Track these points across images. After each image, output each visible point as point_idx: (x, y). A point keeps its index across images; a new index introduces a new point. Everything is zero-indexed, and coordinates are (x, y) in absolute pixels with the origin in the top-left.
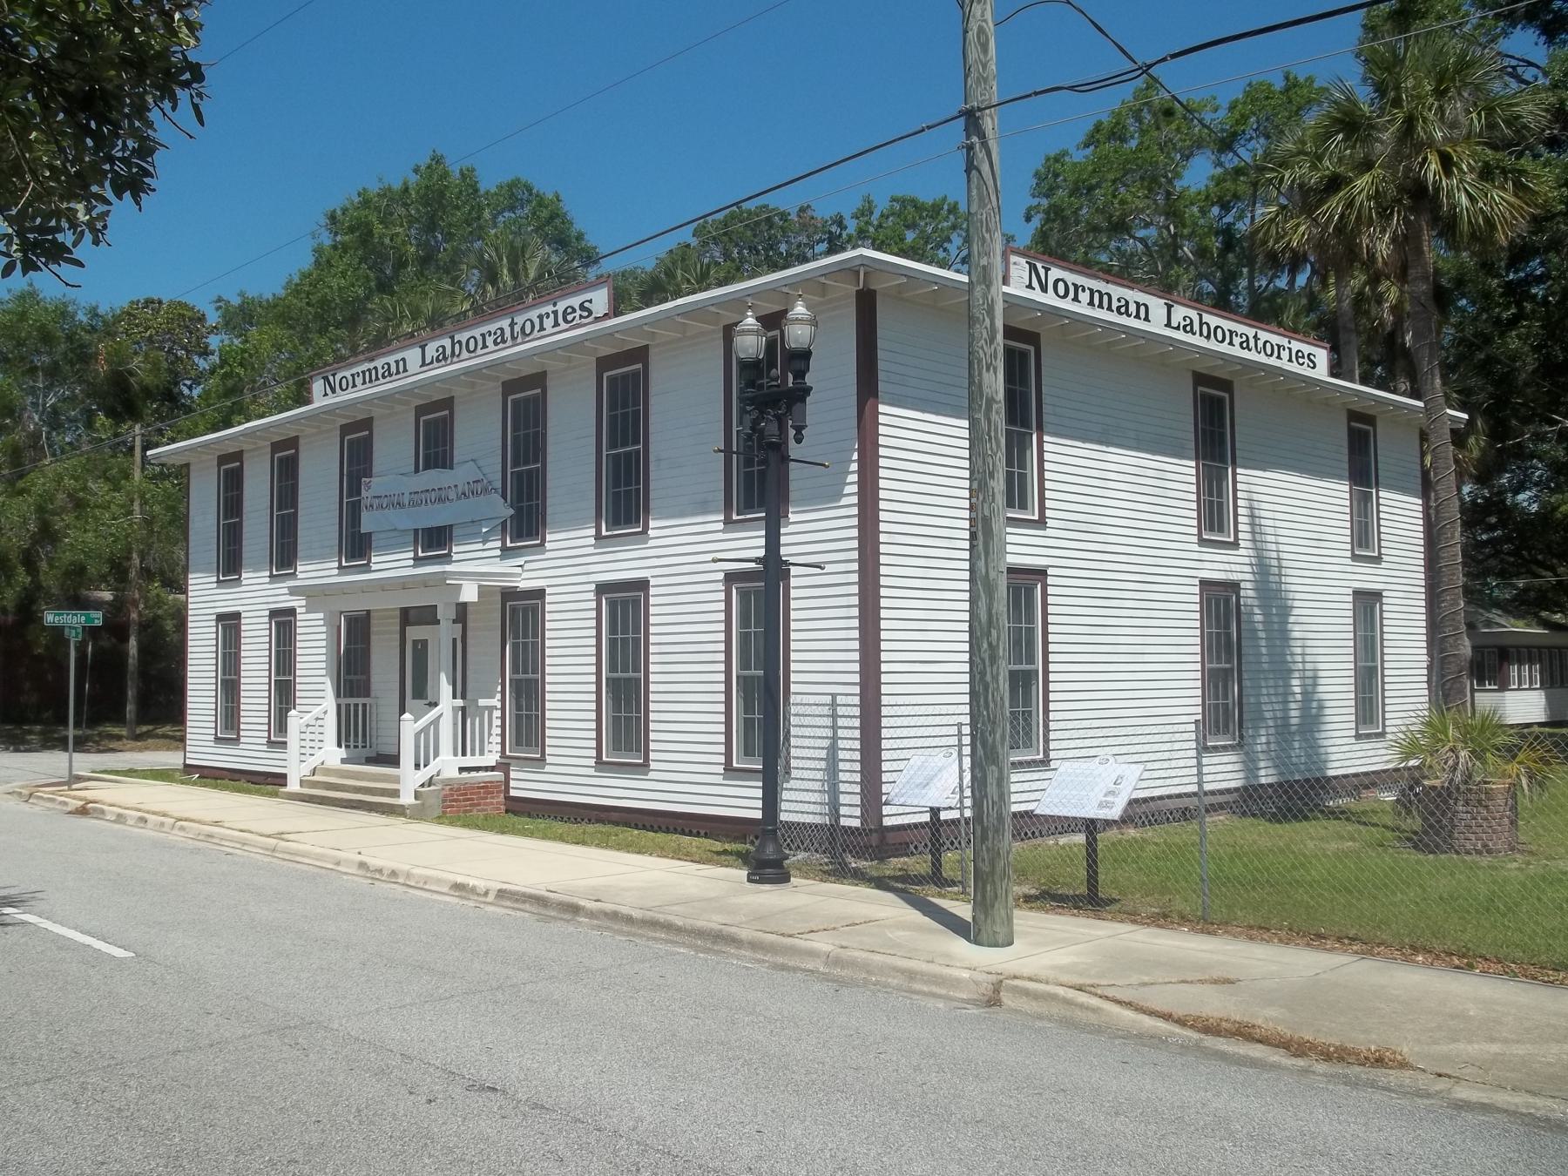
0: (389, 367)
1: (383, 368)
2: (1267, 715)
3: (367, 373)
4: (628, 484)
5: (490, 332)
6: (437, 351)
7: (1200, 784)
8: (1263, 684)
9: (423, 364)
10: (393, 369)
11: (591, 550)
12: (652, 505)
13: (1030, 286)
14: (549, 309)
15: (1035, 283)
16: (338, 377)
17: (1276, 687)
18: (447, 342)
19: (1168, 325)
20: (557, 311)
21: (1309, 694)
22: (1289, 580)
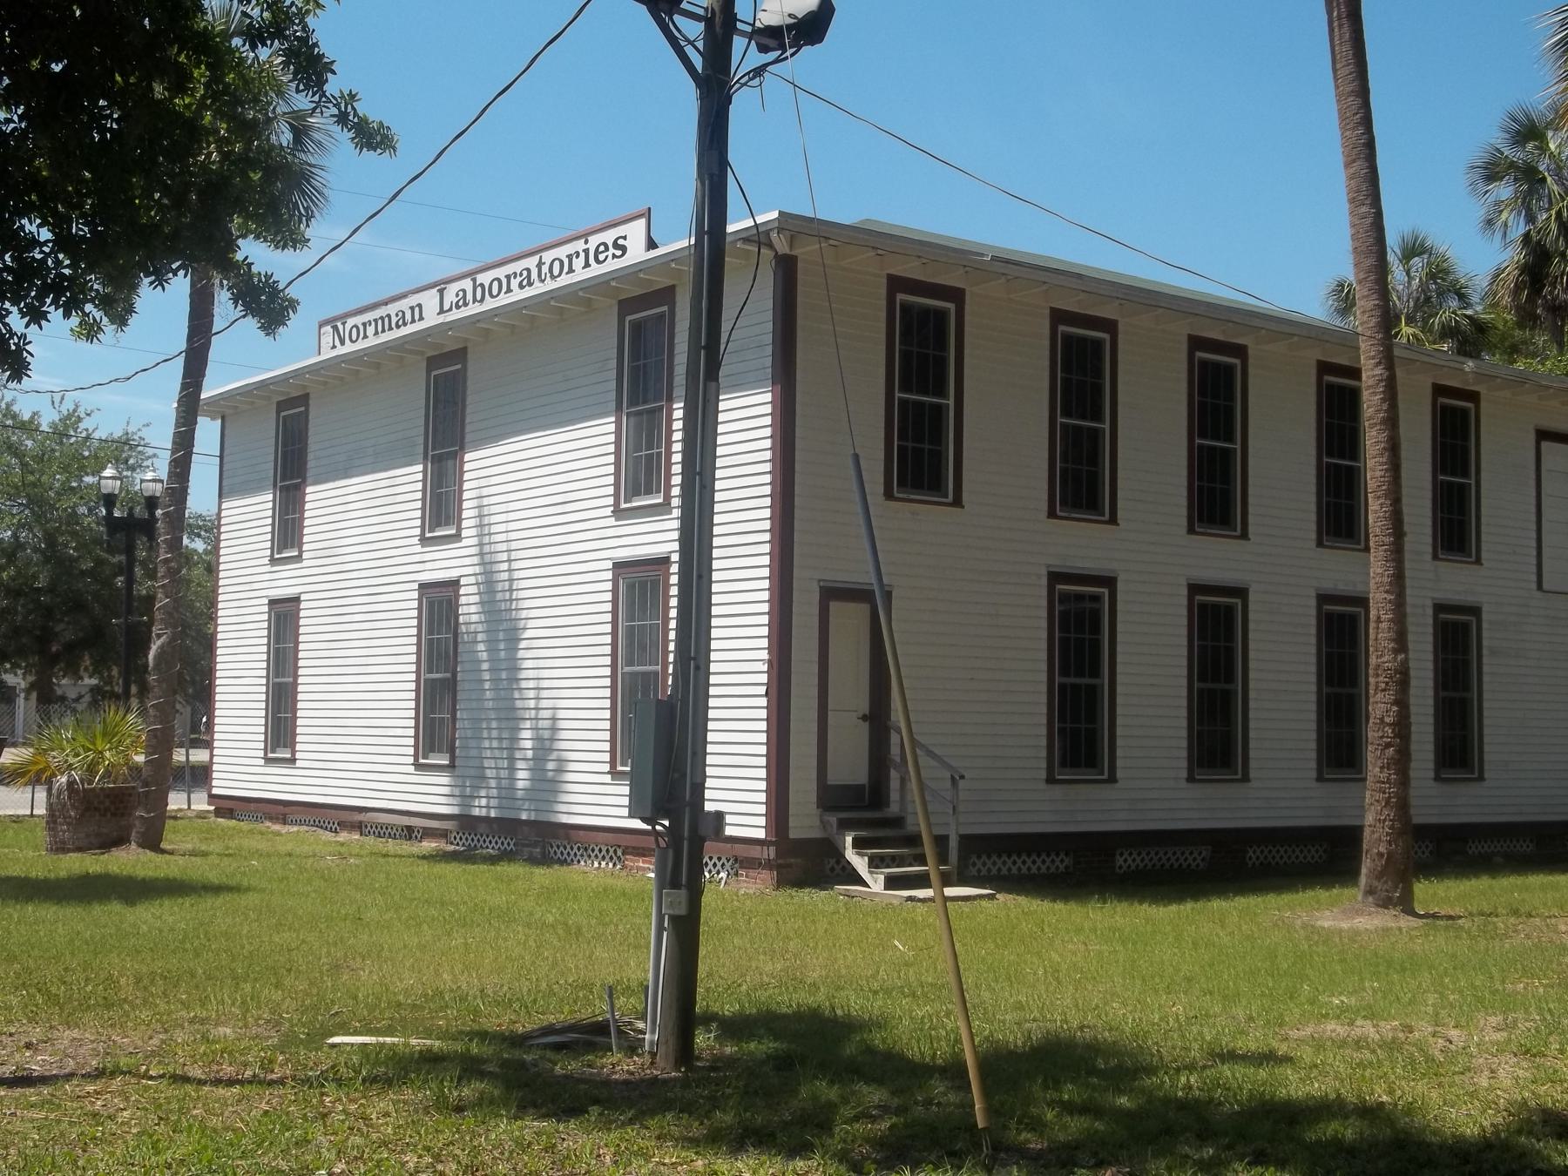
0: (404, 313)
1: (397, 315)
2: (489, 773)
3: (380, 322)
4: (650, 447)
5: (515, 274)
6: (457, 295)
8: (485, 734)
9: (442, 311)
10: (408, 317)
16: (348, 326)
17: (500, 739)
20: (588, 249)
21: (545, 746)
22: (522, 594)
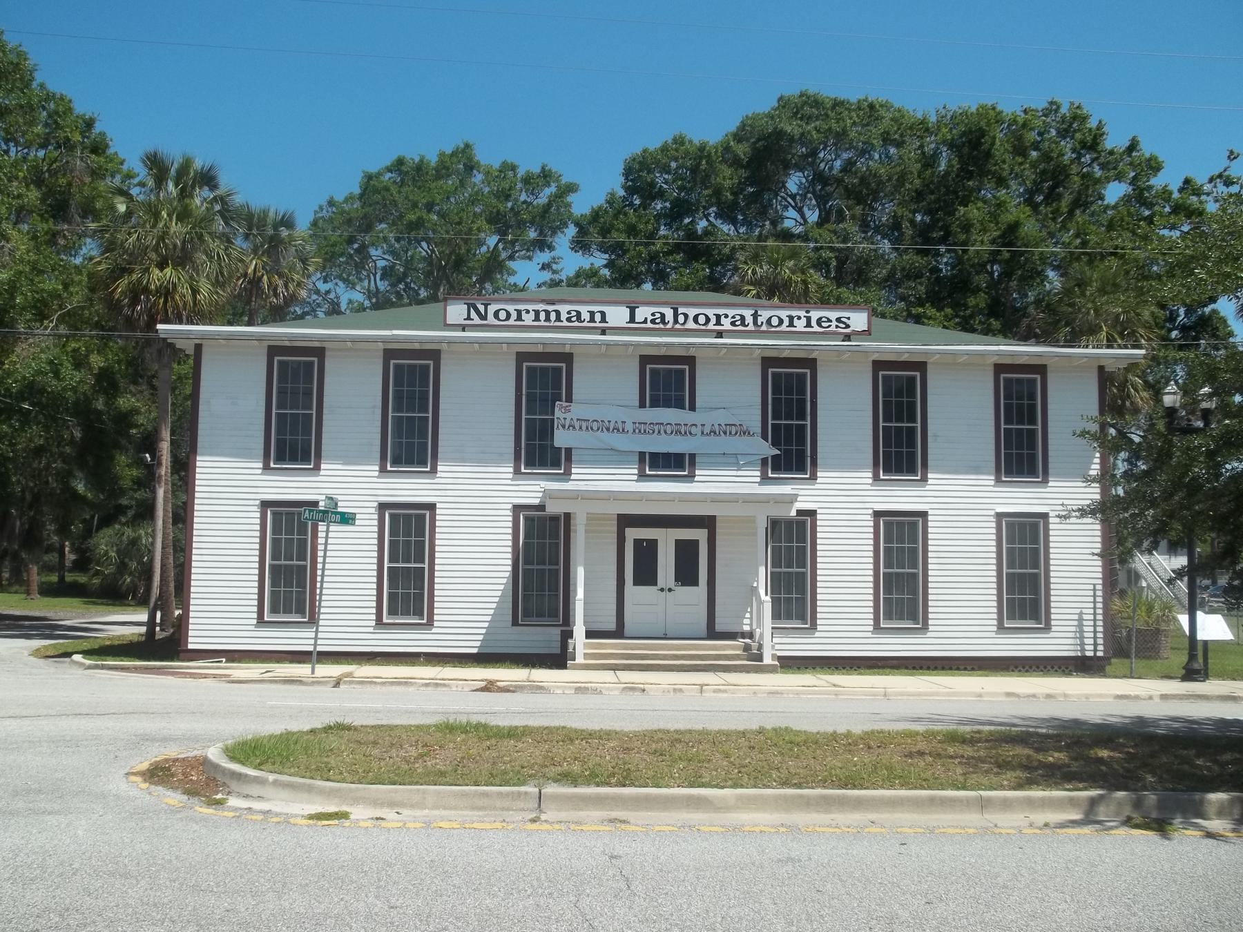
7: (315, 645)
11: (509, 482)
12: (440, 455)
13: (469, 318)
14: (802, 313)
15: (473, 314)
18: (748, 314)
19: (632, 320)
